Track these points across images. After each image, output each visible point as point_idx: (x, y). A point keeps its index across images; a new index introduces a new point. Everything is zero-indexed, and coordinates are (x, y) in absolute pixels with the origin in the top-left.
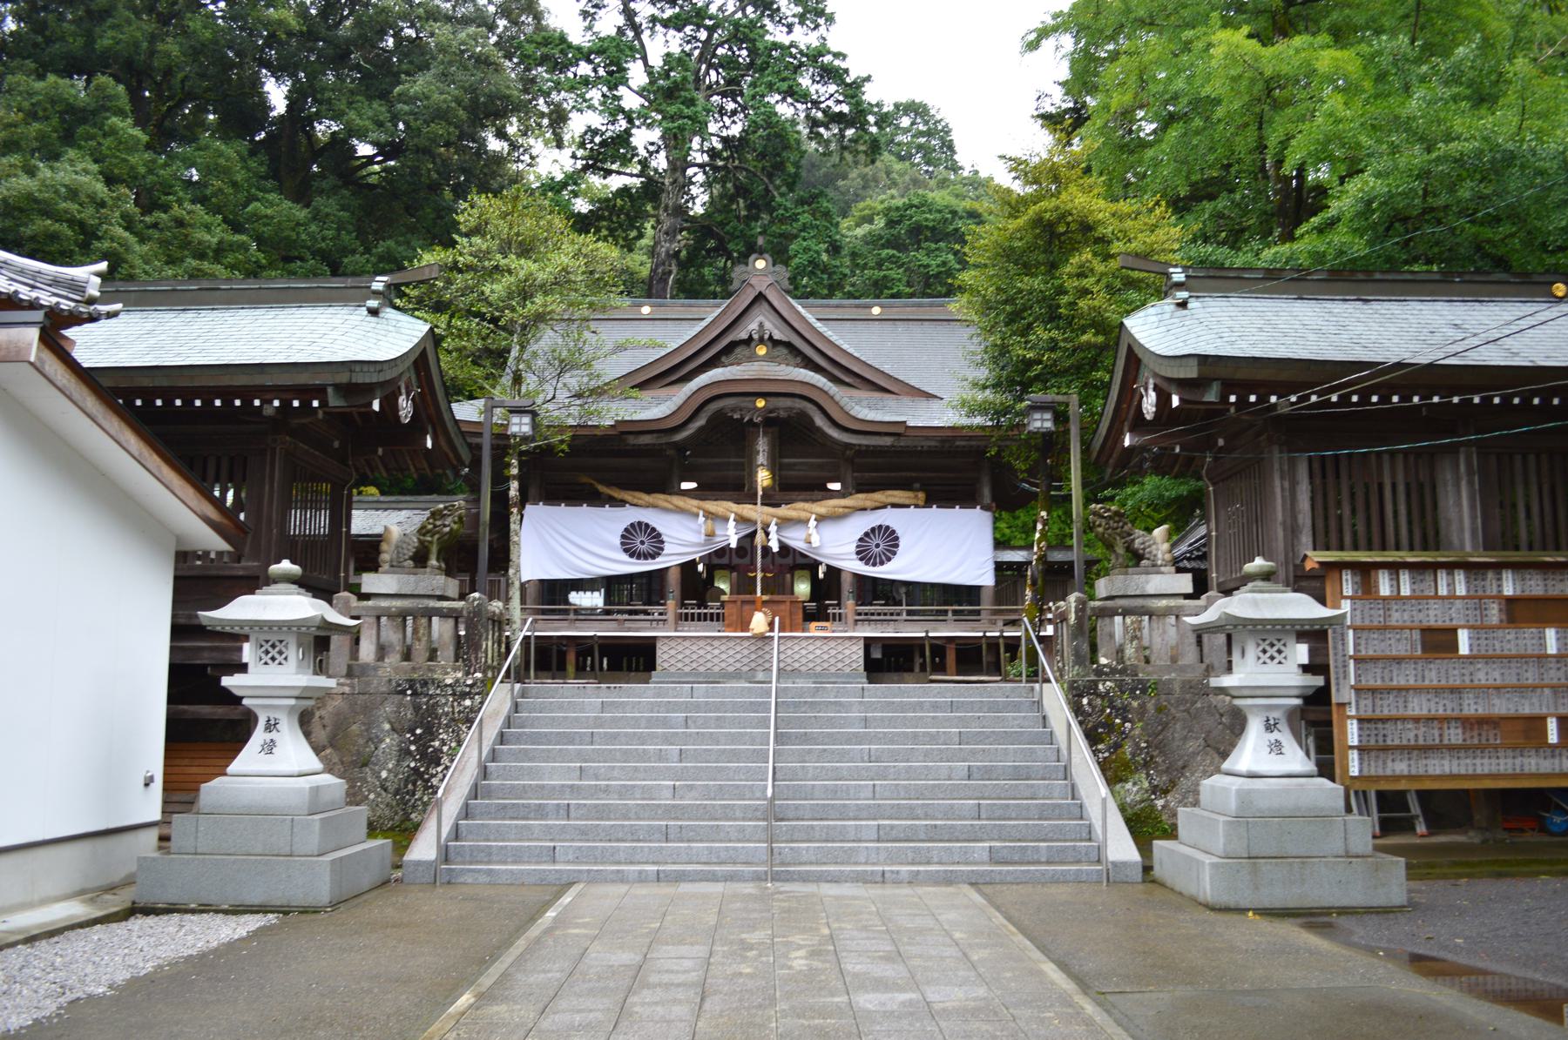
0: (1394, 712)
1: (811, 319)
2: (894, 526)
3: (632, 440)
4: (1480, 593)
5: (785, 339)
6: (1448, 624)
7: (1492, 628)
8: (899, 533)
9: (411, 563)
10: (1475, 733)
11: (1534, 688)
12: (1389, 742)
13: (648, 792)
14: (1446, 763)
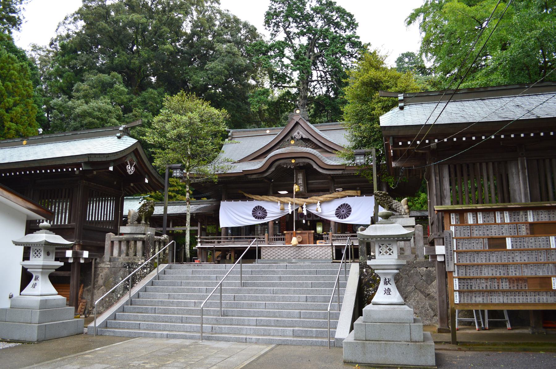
0: (475, 275)
1: (317, 130)
2: (349, 204)
3: (249, 177)
4: (517, 221)
5: (307, 137)
6: (501, 236)
7: (523, 237)
8: (351, 206)
9: (136, 222)
10: (515, 285)
11: (544, 264)
12: (473, 288)
13: (186, 304)
14: (501, 298)
